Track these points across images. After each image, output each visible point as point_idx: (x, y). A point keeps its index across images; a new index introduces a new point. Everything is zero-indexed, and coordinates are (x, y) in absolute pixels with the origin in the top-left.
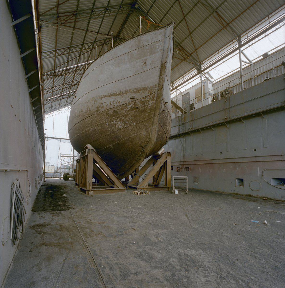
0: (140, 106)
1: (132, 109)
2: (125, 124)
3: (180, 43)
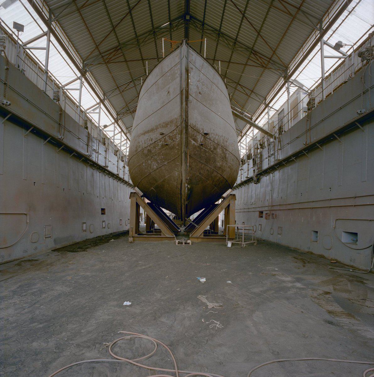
0: (169, 142)
1: (163, 146)
2: (158, 164)
3: (253, 47)
